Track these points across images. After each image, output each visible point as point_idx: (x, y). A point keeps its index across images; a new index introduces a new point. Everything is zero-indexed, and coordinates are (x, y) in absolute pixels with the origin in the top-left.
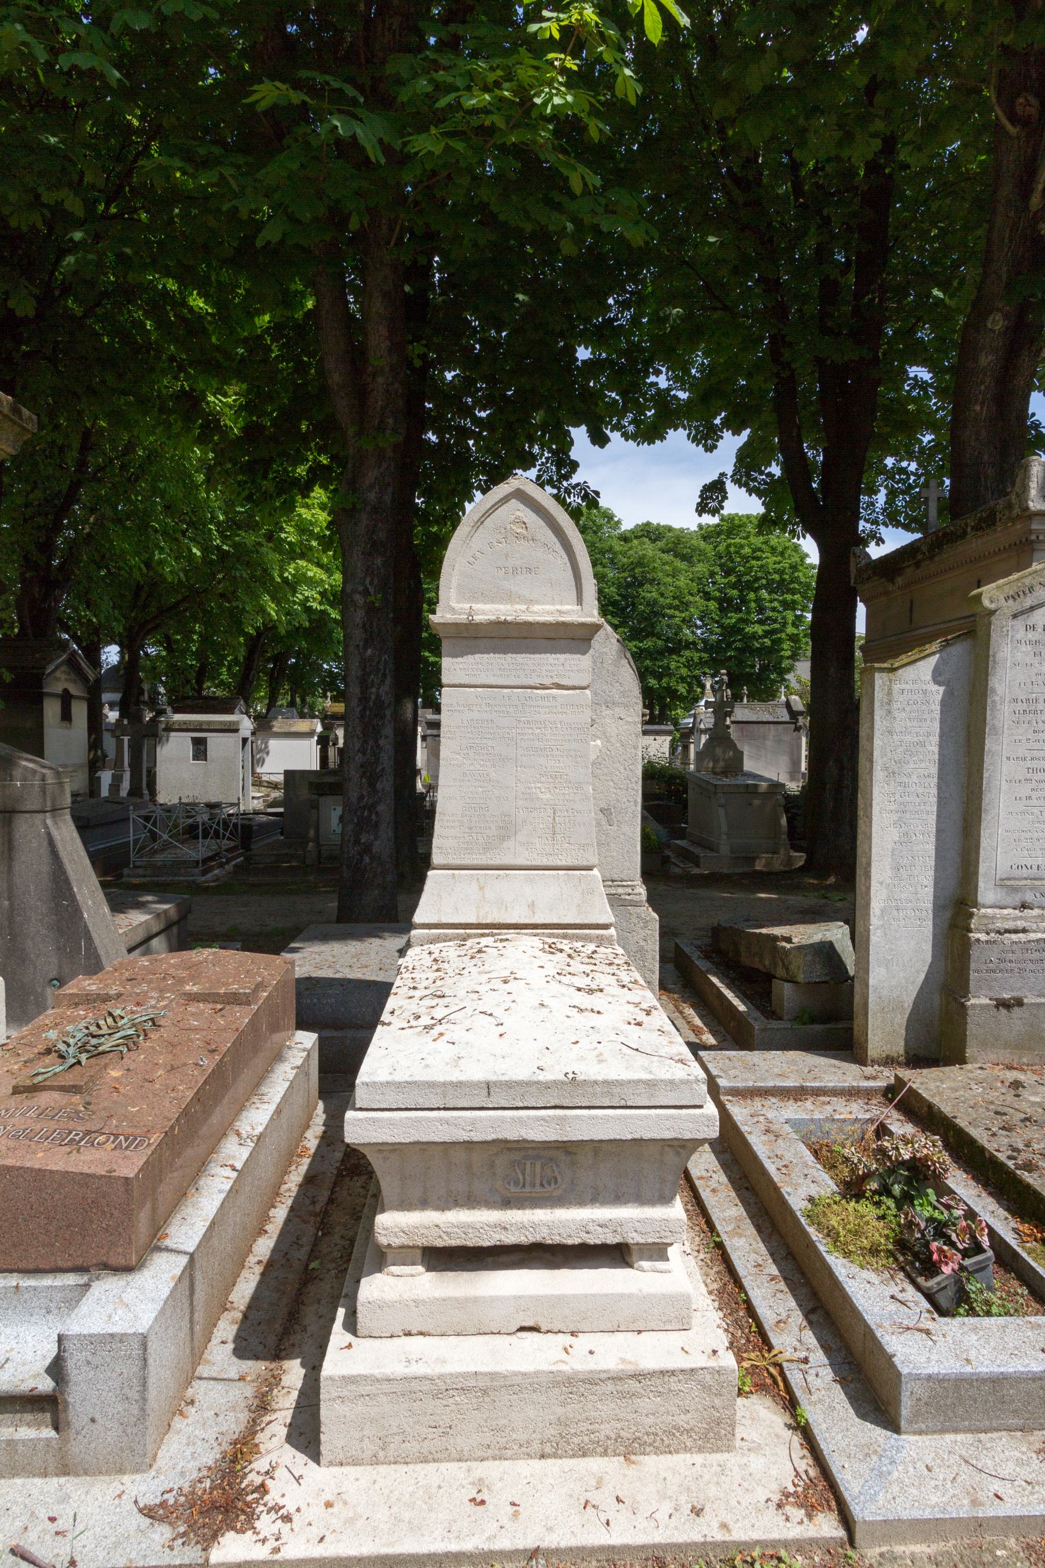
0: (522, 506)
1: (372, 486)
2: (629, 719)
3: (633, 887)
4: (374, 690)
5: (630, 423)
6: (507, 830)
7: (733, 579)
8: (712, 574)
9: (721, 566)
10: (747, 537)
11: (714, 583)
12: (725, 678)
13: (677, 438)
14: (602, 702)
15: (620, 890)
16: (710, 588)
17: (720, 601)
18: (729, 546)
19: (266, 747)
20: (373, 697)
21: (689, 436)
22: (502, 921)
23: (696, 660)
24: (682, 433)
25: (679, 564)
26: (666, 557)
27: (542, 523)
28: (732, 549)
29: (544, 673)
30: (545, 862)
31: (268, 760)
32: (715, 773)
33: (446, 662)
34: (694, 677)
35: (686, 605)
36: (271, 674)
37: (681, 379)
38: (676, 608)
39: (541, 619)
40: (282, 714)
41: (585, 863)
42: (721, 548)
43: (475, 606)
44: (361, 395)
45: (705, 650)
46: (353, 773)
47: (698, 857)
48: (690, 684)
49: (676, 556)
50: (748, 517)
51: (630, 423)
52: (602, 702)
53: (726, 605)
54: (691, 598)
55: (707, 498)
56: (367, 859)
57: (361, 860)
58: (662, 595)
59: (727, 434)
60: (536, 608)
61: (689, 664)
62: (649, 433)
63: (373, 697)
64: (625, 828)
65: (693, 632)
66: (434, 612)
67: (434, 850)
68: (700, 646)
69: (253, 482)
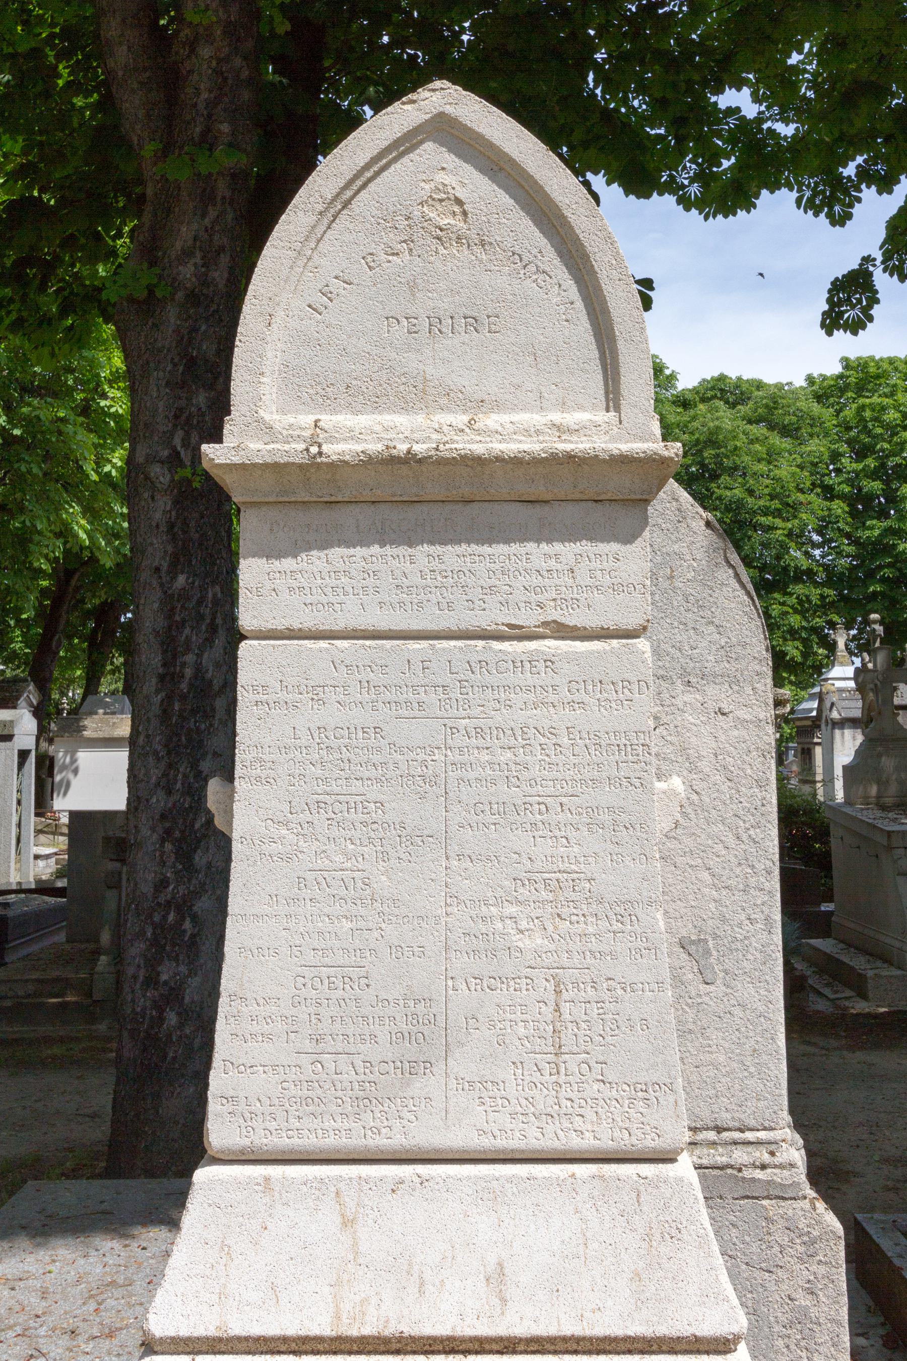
0: (450, 160)
1: (187, 253)
2: (743, 713)
3: (772, 1147)
4: (190, 658)
5: (692, 180)
6: (423, 1042)
7: (871, 463)
8: (835, 456)
9: (849, 442)
10: (892, 394)
11: (838, 471)
12: (879, 629)
13: (778, 207)
14: (679, 672)
15: (740, 1156)
16: (832, 479)
17: (851, 500)
18: (862, 408)
19: (74, 761)
20: (188, 672)
21: (798, 202)
22: (409, 1329)
23: (815, 600)
24: (786, 197)
25: (776, 440)
26: (759, 430)
27: (506, 200)
28: (868, 414)
29: (519, 595)
30: (534, 1138)
31: (75, 782)
32: (883, 808)
33: (251, 572)
34: (815, 630)
35: (794, 508)
36: (92, 639)
37: (779, 89)
38: (777, 513)
39: (510, 448)
40: (106, 706)
41: (650, 1143)
42: (849, 413)
43: (327, 420)
44: (170, 82)
45: (829, 583)
46: (145, 832)
47: (862, 978)
48: (806, 642)
49: (771, 428)
50: (891, 361)
51: (692, 180)
52: (679, 672)
53: (862, 505)
54: (801, 497)
55: (840, 303)
56: (172, 1018)
57: (161, 1019)
58: (751, 492)
59: (869, 194)
60: (492, 421)
61: (803, 608)
62: (727, 197)
63: (188, 672)
64: (747, 991)
65: (807, 553)
66: (217, 437)
67: (214, 1107)
68: (821, 576)
69: (24, 298)
